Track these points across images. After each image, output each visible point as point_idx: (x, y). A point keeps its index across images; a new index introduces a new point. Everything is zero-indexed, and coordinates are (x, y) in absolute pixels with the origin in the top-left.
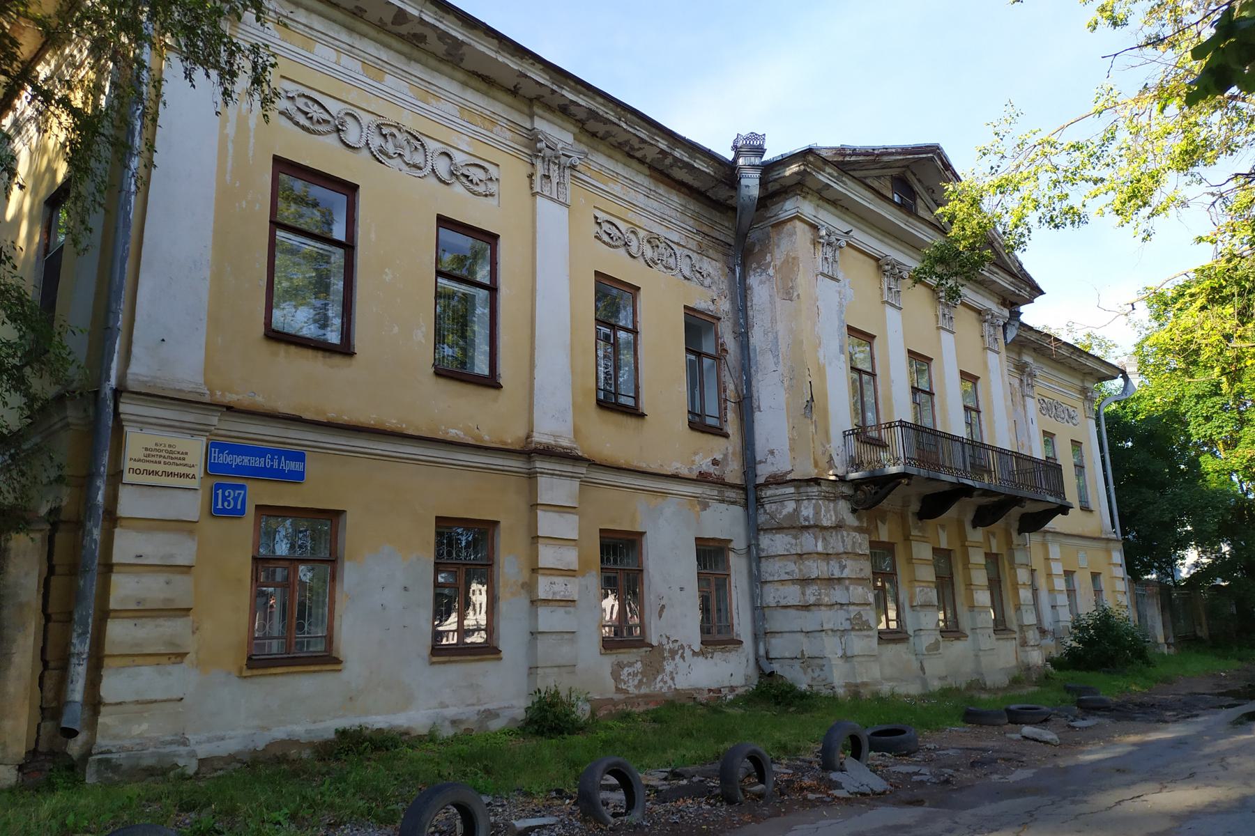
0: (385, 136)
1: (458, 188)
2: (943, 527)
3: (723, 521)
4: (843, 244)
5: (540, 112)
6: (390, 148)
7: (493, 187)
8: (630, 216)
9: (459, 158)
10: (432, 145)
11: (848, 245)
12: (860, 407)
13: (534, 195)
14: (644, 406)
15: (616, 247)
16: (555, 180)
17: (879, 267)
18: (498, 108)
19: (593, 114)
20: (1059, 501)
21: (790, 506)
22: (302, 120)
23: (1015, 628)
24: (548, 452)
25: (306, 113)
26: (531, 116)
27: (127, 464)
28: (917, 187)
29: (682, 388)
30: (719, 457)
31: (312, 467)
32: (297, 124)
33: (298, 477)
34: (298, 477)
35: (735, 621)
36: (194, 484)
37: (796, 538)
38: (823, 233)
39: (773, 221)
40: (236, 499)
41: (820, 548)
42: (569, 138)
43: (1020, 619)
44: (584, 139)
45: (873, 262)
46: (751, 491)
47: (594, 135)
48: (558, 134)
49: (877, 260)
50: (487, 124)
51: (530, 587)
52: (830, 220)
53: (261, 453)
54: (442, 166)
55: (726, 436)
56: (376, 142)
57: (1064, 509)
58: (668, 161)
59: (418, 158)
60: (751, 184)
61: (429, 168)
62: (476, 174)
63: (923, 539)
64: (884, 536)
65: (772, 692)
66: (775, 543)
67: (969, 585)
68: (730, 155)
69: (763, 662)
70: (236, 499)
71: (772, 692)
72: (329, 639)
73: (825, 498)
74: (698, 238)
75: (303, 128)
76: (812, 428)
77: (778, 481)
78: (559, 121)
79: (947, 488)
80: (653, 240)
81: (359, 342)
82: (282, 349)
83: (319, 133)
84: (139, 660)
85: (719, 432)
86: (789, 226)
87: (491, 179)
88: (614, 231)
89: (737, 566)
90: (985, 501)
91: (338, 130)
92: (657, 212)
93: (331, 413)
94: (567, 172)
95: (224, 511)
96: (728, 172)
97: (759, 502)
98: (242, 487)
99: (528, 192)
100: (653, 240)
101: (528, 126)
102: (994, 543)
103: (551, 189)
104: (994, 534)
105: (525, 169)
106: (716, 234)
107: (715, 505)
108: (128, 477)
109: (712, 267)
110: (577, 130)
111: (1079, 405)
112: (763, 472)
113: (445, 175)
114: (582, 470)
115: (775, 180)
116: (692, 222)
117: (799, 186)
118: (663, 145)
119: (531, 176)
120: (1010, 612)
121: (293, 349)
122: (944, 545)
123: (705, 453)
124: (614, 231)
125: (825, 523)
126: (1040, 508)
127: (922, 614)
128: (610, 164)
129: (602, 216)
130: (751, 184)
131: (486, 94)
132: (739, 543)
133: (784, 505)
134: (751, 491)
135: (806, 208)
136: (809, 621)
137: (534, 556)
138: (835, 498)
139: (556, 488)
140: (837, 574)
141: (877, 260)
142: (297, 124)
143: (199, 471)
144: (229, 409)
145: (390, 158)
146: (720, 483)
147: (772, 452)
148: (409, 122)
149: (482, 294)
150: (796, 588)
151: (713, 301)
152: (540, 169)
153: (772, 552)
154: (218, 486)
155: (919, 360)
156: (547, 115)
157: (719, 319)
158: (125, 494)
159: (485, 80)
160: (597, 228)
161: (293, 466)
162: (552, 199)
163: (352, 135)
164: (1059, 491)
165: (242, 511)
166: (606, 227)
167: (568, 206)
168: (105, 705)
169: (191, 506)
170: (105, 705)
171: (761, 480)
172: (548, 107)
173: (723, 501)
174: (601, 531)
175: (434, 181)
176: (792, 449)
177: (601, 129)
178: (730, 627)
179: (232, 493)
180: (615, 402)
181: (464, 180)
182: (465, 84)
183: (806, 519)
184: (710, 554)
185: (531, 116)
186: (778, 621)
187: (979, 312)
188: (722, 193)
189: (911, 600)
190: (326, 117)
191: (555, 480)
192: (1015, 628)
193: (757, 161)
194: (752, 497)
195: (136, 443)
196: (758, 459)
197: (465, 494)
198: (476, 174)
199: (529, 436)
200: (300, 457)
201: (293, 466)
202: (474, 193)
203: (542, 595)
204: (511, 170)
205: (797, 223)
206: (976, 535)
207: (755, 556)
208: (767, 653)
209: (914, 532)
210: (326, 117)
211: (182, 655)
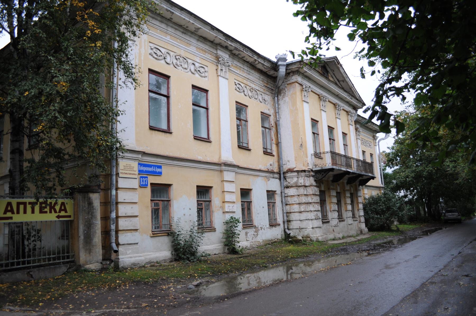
0: (177, 59)
1: (197, 75)
2: (338, 185)
3: (274, 184)
4: (310, 90)
5: (220, 48)
6: (179, 64)
7: (206, 74)
8: (245, 81)
9: (197, 65)
10: (190, 61)
11: (311, 91)
12: (315, 146)
13: (218, 76)
14: (250, 147)
15: (240, 92)
16: (224, 71)
17: (319, 97)
18: (207, 47)
19: (236, 49)
20: (372, 175)
21: (295, 179)
22: (155, 56)
23: (358, 217)
24: (226, 165)
25: (156, 54)
26: (216, 49)
27: (120, 171)
28: (329, 70)
29: (261, 140)
30: (272, 163)
31: (164, 170)
32: (154, 57)
33: (160, 174)
34: (160, 174)
35: (278, 218)
36: (136, 177)
37: (297, 189)
38: (304, 87)
39: (288, 82)
40: (145, 181)
41: (305, 193)
42: (228, 56)
43: (359, 214)
44: (231, 56)
45: (317, 96)
46: (281, 174)
47: (235, 54)
48: (224, 55)
49: (319, 95)
50: (204, 52)
51: (222, 207)
52: (306, 83)
53: (150, 166)
54: (192, 68)
55: (274, 156)
56: (175, 61)
57: (373, 178)
58: (257, 62)
59: (186, 66)
60: (282, 70)
61: (189, 69)
62: (202, 70)
63: (333, 189)
64: (323, 189)
65: (288, 239)
66: (291, 192)
67: (346, 204)
68: (275, 60)
69: (287, 230)
70: (145, 181)
71: (288, 239)
72: (211, 222)
73: (307, 176)
74: (264, 88)
75: (156, 58)
76: (302, 153)
77: (291, 171)
78: (225, 51)
79: (342, 172)
80: (252, 90)
81: (173, 128)
82: (154, 132)
83: (158, 60)
84: (127, 231)
85: (271, 154)
86: (293, 85)
87: (206, 71)
88: (240, 87)
89: (278, 199)
90: (351, 176)
91: (165, 58)
92: (255, 81)
93: (171, 154)
94: (227, 67)
95: (143, 185)
96: (275, 66)
97: (285, 178)
98: (147, 177)
99: (216, 75)
100: (252, 90)
101: (215, 52)
102: (352, 189)
103: (223, 74)
104: (352, 186)
105: (215, 67)
106: (268, 86)
107: (271, 179)
108: (120, 175)
109: (268, 98)
110: (229, 53)
111: (372, 141)
112: (285, 168)
113: (193, 71)
114: (236, 169)
115: (290, 69)
116: (262, 82)
117: (297, 72)
118: (256, 58)
119: (217, 70)
120: (356, 212)
121: (156, 132)
122: (339, 191)
123: (268, 163)
124: (240, 87)
125: (307, 185)
126: (367, 177)
127: (333, 214)
128: (238, 64)
129: (237, 82)
130: (282, 70)
131: (204, 43)
132: (278, 192)
133: (292, 179)
134: (281, 174)
135: (299, 79)
136: (303, 216)
137: (224, 198)
138: (309, 177)
139: (229, 175)
140: (310, 201)
141: (319, 95)
142: (154, 57)
143: (137, 172)
144: (144, 154)
145: (179, 66)
146: (272, 172)
147: (289, 161)
148: (183, 54)
149: (203, 110)
150: (297, 206)
151: (269, 110)
152: (220, 68)
153: (290, 194)
154: (141, 177)
155: (331, 129)
156: (222, 49)
157: (270, 116)
158: (120, 180)
159: (204, 39)
160: (235, 86)
161: (158, 170)
162: (223, 77)
163: (168, 60)
164: (372, 172)
165: (147, 185)
166: (238, 85)
167: (227, 79)
168: (120, 245)
169: (135, 184)
170: (120, 245)
171: (285, 170)
172: (222, 46)
173: (274, 178)
174: (197, 186)
175: (190, 73)
176: (296, 160)
177: (237, 52)
178: (276, 219)
179: (144, 179)
180: (243, 147)
181: (198, 72)
182: (198, 40)
183: (301, 183)
184: (271, 194)
185: (216, 49)
186: (294, 217)
187: (347, 112)
188: (272, 73)
189: (330, 209)
190: (161, 54)
191: (229, 172)
192: (358, 217)
193: (285, 63)
194: (282, 176)
195: (122, 163)
196: (284, 163)
197: (205, 178)
198: (202, 70)
199: (220, 157)
200: (160, 167)
201: (158, 170)
202: (201, 76)
203: (227, 210)
204: (211, 68)
205: (297, 84)
206: (347, 187)
207: (284, 196)
208: (288, 227)
209: (331, 187)
210: (161, 54)
211: (137, 230)
